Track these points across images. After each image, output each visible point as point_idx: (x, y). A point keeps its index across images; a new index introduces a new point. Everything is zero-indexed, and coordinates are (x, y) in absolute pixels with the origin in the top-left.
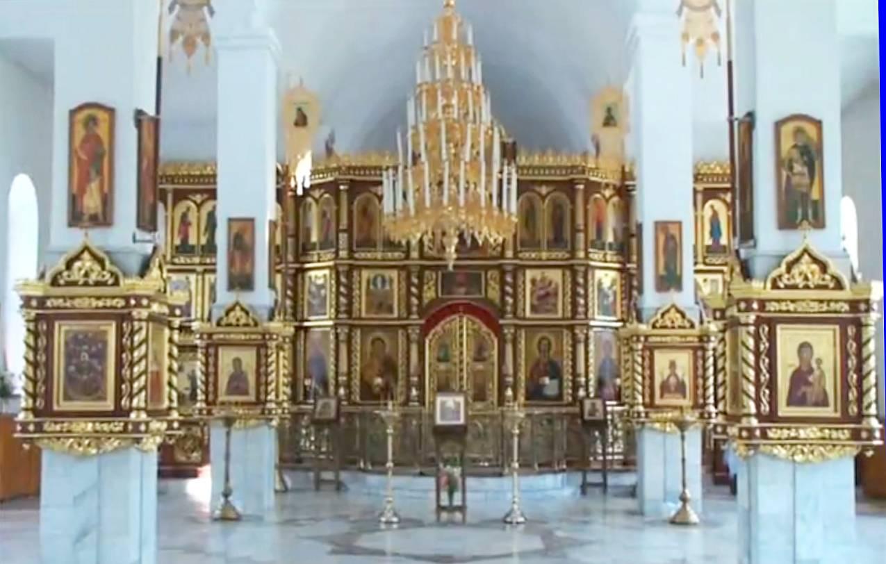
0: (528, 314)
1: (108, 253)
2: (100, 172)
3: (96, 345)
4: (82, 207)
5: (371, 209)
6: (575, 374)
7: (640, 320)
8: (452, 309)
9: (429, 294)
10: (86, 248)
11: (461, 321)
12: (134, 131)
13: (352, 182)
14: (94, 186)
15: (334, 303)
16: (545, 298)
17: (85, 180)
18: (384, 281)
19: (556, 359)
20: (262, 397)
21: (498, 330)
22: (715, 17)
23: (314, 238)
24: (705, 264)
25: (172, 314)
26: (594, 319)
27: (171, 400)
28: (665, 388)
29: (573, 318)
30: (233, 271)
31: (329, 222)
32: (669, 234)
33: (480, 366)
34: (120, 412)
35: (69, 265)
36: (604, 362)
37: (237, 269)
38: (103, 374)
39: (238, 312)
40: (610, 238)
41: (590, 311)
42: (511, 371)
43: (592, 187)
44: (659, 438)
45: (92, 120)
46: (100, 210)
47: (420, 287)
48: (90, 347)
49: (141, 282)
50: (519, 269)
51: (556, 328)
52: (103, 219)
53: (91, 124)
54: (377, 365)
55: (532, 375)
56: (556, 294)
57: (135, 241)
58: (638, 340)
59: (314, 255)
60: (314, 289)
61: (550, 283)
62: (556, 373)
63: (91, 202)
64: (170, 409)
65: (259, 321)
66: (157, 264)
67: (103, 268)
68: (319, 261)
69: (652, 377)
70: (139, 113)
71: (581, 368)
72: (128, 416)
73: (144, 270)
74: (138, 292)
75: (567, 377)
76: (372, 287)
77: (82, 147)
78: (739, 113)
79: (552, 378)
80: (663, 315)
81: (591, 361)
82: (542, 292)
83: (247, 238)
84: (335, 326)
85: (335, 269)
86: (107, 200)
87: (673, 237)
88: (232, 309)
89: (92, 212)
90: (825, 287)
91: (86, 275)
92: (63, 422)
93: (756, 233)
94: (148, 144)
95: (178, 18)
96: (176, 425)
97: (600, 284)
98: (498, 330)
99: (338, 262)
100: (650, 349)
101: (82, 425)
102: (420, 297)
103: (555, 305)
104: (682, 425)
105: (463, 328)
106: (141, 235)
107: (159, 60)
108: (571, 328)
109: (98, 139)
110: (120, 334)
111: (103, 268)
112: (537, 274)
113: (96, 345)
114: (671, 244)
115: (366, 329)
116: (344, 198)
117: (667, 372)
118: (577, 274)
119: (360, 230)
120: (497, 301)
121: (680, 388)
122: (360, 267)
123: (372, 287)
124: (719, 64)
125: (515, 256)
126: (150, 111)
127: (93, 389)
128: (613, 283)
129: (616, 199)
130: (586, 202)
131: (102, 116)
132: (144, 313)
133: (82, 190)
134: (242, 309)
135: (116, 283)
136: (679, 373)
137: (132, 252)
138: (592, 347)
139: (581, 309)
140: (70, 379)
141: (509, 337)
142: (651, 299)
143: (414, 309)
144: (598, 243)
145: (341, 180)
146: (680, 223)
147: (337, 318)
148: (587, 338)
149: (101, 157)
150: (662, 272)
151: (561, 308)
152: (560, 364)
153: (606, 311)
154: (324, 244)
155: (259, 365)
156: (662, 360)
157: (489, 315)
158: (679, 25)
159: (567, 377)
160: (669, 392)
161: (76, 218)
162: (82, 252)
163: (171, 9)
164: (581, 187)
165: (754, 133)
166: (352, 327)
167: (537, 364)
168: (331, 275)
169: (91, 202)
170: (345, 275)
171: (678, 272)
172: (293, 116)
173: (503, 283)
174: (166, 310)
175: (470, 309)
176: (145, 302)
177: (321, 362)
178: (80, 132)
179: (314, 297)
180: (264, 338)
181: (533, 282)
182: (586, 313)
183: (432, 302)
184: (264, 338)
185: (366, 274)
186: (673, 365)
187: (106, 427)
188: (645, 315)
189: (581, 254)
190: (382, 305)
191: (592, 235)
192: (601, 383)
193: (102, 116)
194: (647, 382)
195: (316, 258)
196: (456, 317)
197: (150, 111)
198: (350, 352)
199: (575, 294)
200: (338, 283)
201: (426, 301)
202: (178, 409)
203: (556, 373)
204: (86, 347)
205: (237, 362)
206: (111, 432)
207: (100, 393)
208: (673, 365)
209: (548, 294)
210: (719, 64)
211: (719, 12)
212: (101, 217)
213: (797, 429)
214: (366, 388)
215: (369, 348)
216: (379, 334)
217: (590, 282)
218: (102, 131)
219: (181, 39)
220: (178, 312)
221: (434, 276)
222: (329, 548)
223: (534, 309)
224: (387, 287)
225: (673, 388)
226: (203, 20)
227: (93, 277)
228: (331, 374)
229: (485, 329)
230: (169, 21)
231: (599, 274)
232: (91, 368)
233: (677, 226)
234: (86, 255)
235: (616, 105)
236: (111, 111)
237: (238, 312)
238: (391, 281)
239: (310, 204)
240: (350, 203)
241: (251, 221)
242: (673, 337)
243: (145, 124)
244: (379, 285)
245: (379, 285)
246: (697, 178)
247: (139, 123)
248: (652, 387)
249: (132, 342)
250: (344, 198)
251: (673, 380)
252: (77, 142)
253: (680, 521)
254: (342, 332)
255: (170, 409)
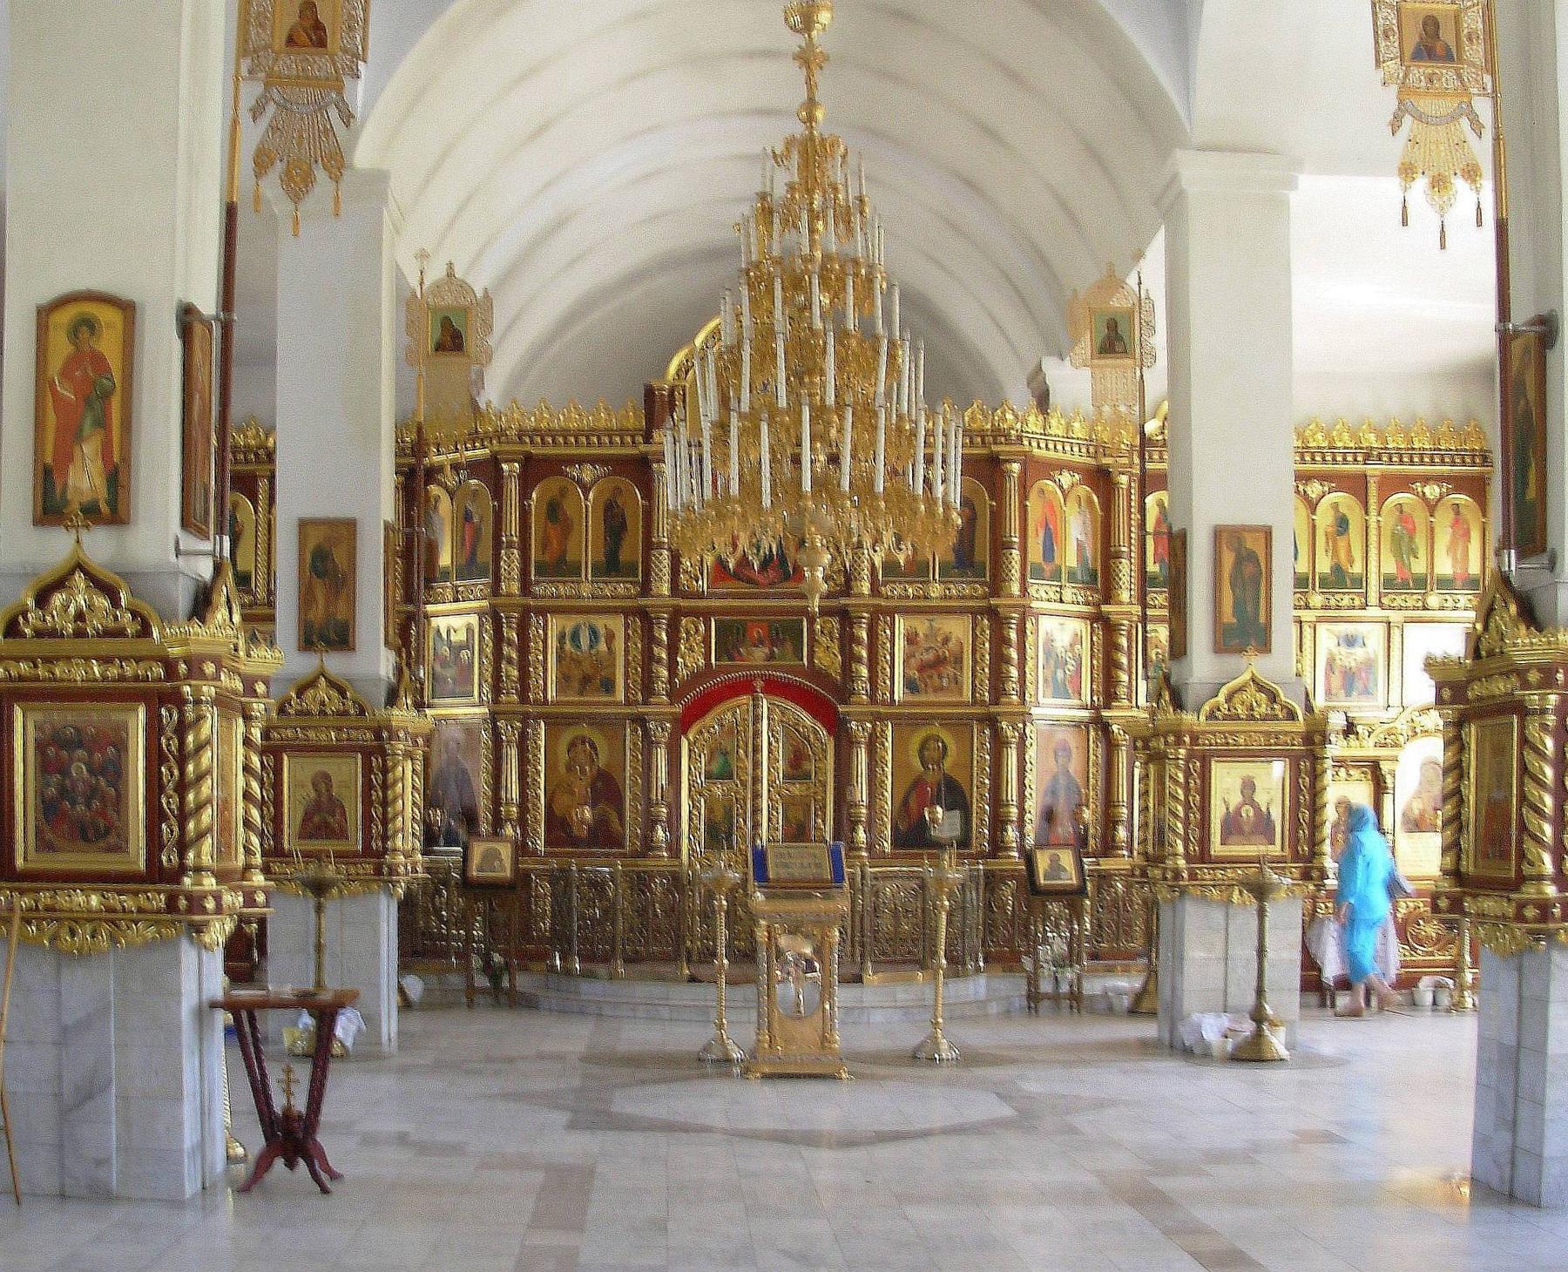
0: (899, 692)
1: (126, 576)
2: (102, 423)
3: (102, 750)
4: (65, 485)
5: (568, 507)
6: (997, 801)
7: (1178, 704)
8: (745, 687)
9: (691, 660)
10: (79, 566)
11: (755, 706)
12: (177, 345)
13: (528, 461)
14: (90, 448)
15: (488, 675)
16: (932, 666)
17: (70, 437)
18: (594, 633)
19: (960, 778)
20: (168, 858)
21: (836, 726)
22: (1471, 136)
23: (445, 559)
24: (1381, 605)
25: (250, 690)
26: (1038, 705)
27: (248, 851)
28: (1232, 827)
29: (995, 701)
30: (311, 616)
31: (477, 533)
32: (1245, 555)
33: (797, 789)
34: (156, 874)
35: (42, 599)
36: (1055, 779)
37: (318, 613)
38: (120, 801)
39: (80, 595)
40: (1072, 561)
41: (1030, 688)
42: (515, 793)
43: (1037, 469)
44: (1218, 915)
45: (88, 325)
46: (102, 494)
47: (673, 649)
48: (91, 754)
49: (195, 628)
50: (881, 614)
51: (609, 725)
52: (113, 509)
53: (85, 332)
54: (581, 787)
55: (905, 803)
56: (958, 660)
57: (178, 553)
58: (1179, 742)
59: (445, 588)
60: (445, 650)
61: (946, 640)
62: (955, 797)
63: (85, 480)
64: (248, 867)
65: (367, 706)
66: (223, 599)
67: (115, 603)
68: (456, 600)
69: (1205, 809)
70: (187, 317)
71: (861, 792)
72: (178, 882)
73: (202, 604)
74: (194, 649)
75: (980, 807)
76: (568, 646)
77: (66, 373)
78: (1521, 315)
79: (948, 808)
80: (1229, 699)
81: (1030, 778)
82: (929, 656)
83: (339, 556)
84: (494, 717)
85: (494, 617)
86: (117, 477)
87: (1252, 557)
88: (312, 684)
89: (86, 499)
90: (1275, 718)
91: (80, 616)
92: (37, 891)
93: (1551, 542)
94: (208, 376)
95: (273, 128)
96: (260, 898)
97: (1050, 641)
98: (836, 726)
99: (499, 601)
100: (1203, 761)
101: (80, 898)
102: (672, 667)
103: (957, 681)
104: (1261, 891)
105: (769, 725)
106: (189, 542)
107: (230, 212)
108: (991, 721)
109: (99, 361)
110: (154, 729)
111: (115, 603)
112: (921, 625)
113: (102, 750)
114: (1248, 569)
115: (556, 722)
116: (513, 488)
117: (1236, 799)
118: (1000, 626)
119: (545, 545)
120: (835, 672)
121: (1263, 826)
122: (543, 612)
123: (568, 646)
124: (1479, 223)
125: (875, 591)
126: (207, 303)
127: (102, 829)
128: (1077, 640)
129: (1084, 490)
130: (1024, 497)
131: (108, 316)
132: (208, 691)
133: (65, 457)
134: (332, 684)
135: (145, 631)
136: (1261, 798)
137: (176, 573)
138: (1031, 753)
139: (1012, 686)
140: (50, 810)
141: (863, 737)
142: (1202, 664)
143: (661, 686)
144: (1047, 568)
145: (508, 452)
146: (1268, 533)
147: (496, 701)
148: (1023, 737)
149: (106, 395)
150: (1228, 616)
151: (969, 685)
152: (966, 788)
153: (1059, 691)
154: (468, 568)
155: (368, 786)
156: (1226, 781)
157: (824, 700)
158: (1397, 147)
159: (980, 807)
160: (1241, 832)
161: (50, 509)
162: (72, 572)
163: (256, 112)
164: (1016, 467)
165: (1551, 357)
166: (525, 717)
167: (918, 784)
168: (481, 625)
169: (85, 480)
170: (509, 628)
171: (1262, 620)
172: (432, 334)
173: (847, 641)
174: (239, 686)
175: (775, 687)
176: (210, 668)
177: (464, 780)
178: (61, 349)
179: (444, 664)
180: (378, 737)
181: (911, 639)
182: (1022, 695)
183: (697, 677)
184: (378, 737)
185: (555, 624)
186: (1249, 787)
187: (129, 902)
188: (1190, 698)
189: (1015, 589)
190: (593, 678)
191: (1035, 554)
192: (1049, 816)
193: (108, 316)
194: (1195, 817)
195: (449, 594)
196: (745, 699)
197: (207, 303)
198: (523, 761)
199: (999, 660)
200: (498, 638)
201: (683, 672)
202: (266, 870)
203: (955, 797)
204: (81, 753)
205: (322, 781)
206: (140, 910)
207: (112, 840)
208: (1249, 787)
209: (939, 662)
210: (1479, 223)
211: (1477, 128)
212: (104, 508)
213: (105, 678)
214: (558, 827)
215: (563, 756)
216: (584, 730)
217: (1030, 639)
218: (108, 345)
219: (279, 167)
220: (260, 688)
221: (702, 628)
222: (562, 1118)
223: (910, 685)
224: (603, 647)
225: (1247, 829)
226: (329, 131)
227: (95, 623)
228: (483, 804)
229: (807, 719)
230: (252, 135)
231: (1046, 624)
232: (93, 792)
233: (1262, 535)
234: (79, 578)
235: (1130, 315)
236: (127, 308)
237: (322, 691)
238: (610, 637)
239: (437, 499)
240: (525, 495)
241: (350, 526)
242: (1248, 733)
243: (198, 329)
244: (584, 641)
245: (584, 641)
246: (1304, 452)
247: (186, 333)
248: (1205, 824)
249: (182, 742)
250: (513, 488)
251: (1248, 812)
252: (55, 365)
253: (1251, 1053)
254: (509, 731)
255: (248, 867)
